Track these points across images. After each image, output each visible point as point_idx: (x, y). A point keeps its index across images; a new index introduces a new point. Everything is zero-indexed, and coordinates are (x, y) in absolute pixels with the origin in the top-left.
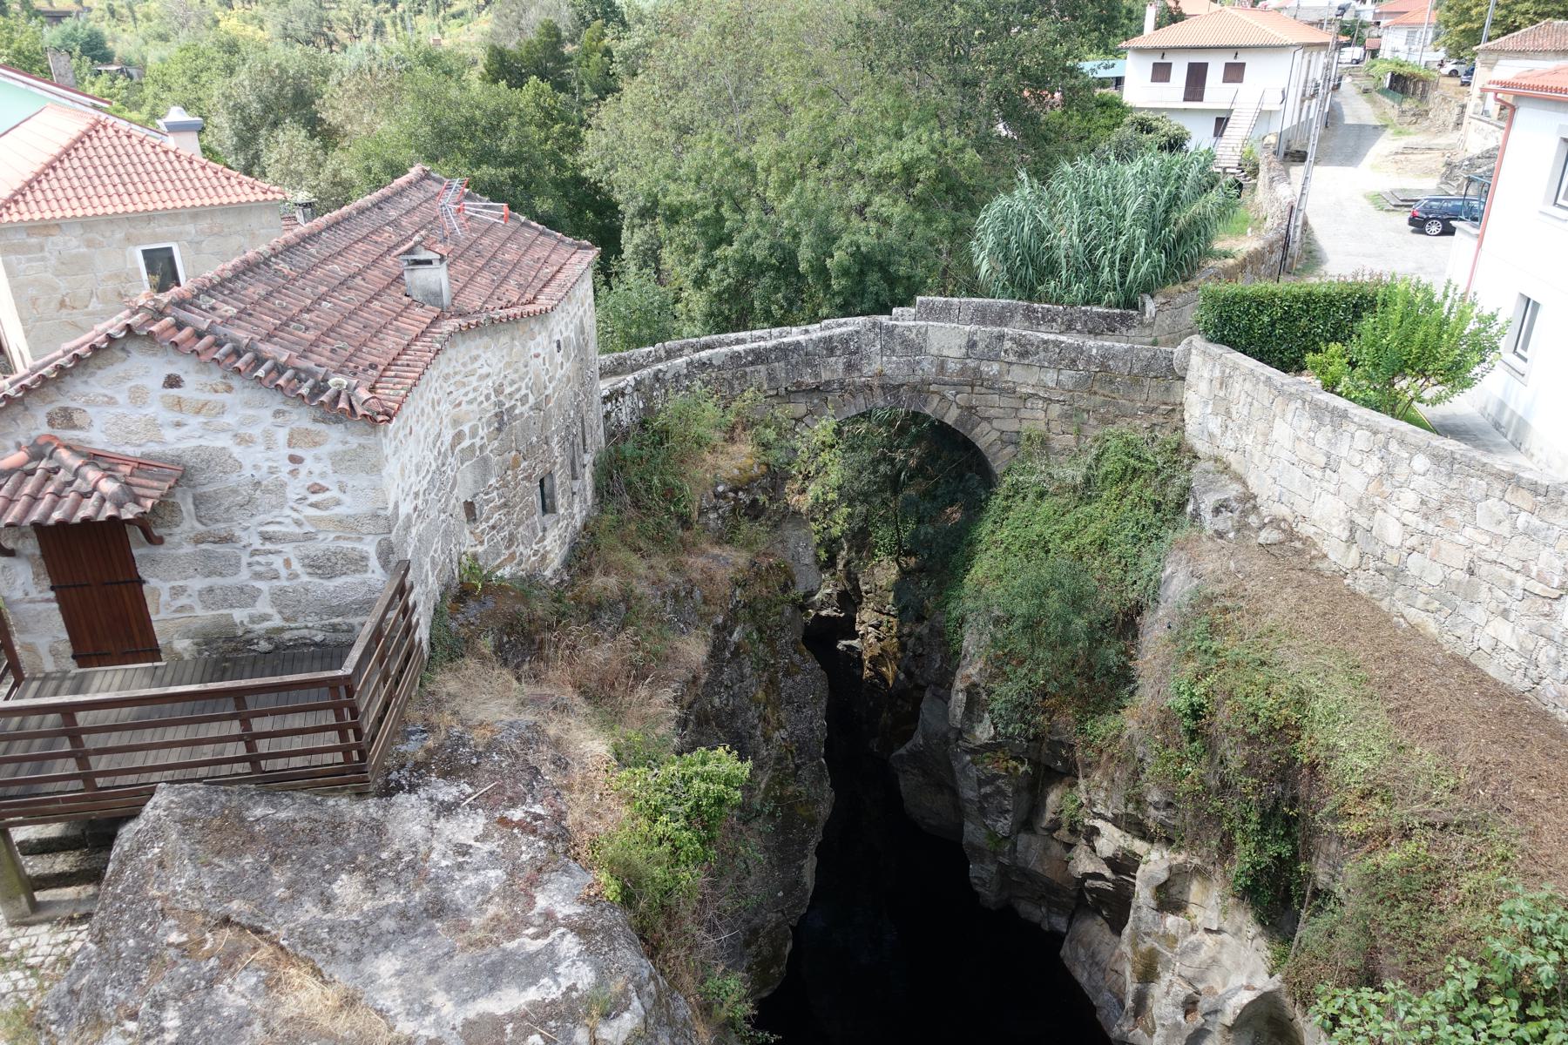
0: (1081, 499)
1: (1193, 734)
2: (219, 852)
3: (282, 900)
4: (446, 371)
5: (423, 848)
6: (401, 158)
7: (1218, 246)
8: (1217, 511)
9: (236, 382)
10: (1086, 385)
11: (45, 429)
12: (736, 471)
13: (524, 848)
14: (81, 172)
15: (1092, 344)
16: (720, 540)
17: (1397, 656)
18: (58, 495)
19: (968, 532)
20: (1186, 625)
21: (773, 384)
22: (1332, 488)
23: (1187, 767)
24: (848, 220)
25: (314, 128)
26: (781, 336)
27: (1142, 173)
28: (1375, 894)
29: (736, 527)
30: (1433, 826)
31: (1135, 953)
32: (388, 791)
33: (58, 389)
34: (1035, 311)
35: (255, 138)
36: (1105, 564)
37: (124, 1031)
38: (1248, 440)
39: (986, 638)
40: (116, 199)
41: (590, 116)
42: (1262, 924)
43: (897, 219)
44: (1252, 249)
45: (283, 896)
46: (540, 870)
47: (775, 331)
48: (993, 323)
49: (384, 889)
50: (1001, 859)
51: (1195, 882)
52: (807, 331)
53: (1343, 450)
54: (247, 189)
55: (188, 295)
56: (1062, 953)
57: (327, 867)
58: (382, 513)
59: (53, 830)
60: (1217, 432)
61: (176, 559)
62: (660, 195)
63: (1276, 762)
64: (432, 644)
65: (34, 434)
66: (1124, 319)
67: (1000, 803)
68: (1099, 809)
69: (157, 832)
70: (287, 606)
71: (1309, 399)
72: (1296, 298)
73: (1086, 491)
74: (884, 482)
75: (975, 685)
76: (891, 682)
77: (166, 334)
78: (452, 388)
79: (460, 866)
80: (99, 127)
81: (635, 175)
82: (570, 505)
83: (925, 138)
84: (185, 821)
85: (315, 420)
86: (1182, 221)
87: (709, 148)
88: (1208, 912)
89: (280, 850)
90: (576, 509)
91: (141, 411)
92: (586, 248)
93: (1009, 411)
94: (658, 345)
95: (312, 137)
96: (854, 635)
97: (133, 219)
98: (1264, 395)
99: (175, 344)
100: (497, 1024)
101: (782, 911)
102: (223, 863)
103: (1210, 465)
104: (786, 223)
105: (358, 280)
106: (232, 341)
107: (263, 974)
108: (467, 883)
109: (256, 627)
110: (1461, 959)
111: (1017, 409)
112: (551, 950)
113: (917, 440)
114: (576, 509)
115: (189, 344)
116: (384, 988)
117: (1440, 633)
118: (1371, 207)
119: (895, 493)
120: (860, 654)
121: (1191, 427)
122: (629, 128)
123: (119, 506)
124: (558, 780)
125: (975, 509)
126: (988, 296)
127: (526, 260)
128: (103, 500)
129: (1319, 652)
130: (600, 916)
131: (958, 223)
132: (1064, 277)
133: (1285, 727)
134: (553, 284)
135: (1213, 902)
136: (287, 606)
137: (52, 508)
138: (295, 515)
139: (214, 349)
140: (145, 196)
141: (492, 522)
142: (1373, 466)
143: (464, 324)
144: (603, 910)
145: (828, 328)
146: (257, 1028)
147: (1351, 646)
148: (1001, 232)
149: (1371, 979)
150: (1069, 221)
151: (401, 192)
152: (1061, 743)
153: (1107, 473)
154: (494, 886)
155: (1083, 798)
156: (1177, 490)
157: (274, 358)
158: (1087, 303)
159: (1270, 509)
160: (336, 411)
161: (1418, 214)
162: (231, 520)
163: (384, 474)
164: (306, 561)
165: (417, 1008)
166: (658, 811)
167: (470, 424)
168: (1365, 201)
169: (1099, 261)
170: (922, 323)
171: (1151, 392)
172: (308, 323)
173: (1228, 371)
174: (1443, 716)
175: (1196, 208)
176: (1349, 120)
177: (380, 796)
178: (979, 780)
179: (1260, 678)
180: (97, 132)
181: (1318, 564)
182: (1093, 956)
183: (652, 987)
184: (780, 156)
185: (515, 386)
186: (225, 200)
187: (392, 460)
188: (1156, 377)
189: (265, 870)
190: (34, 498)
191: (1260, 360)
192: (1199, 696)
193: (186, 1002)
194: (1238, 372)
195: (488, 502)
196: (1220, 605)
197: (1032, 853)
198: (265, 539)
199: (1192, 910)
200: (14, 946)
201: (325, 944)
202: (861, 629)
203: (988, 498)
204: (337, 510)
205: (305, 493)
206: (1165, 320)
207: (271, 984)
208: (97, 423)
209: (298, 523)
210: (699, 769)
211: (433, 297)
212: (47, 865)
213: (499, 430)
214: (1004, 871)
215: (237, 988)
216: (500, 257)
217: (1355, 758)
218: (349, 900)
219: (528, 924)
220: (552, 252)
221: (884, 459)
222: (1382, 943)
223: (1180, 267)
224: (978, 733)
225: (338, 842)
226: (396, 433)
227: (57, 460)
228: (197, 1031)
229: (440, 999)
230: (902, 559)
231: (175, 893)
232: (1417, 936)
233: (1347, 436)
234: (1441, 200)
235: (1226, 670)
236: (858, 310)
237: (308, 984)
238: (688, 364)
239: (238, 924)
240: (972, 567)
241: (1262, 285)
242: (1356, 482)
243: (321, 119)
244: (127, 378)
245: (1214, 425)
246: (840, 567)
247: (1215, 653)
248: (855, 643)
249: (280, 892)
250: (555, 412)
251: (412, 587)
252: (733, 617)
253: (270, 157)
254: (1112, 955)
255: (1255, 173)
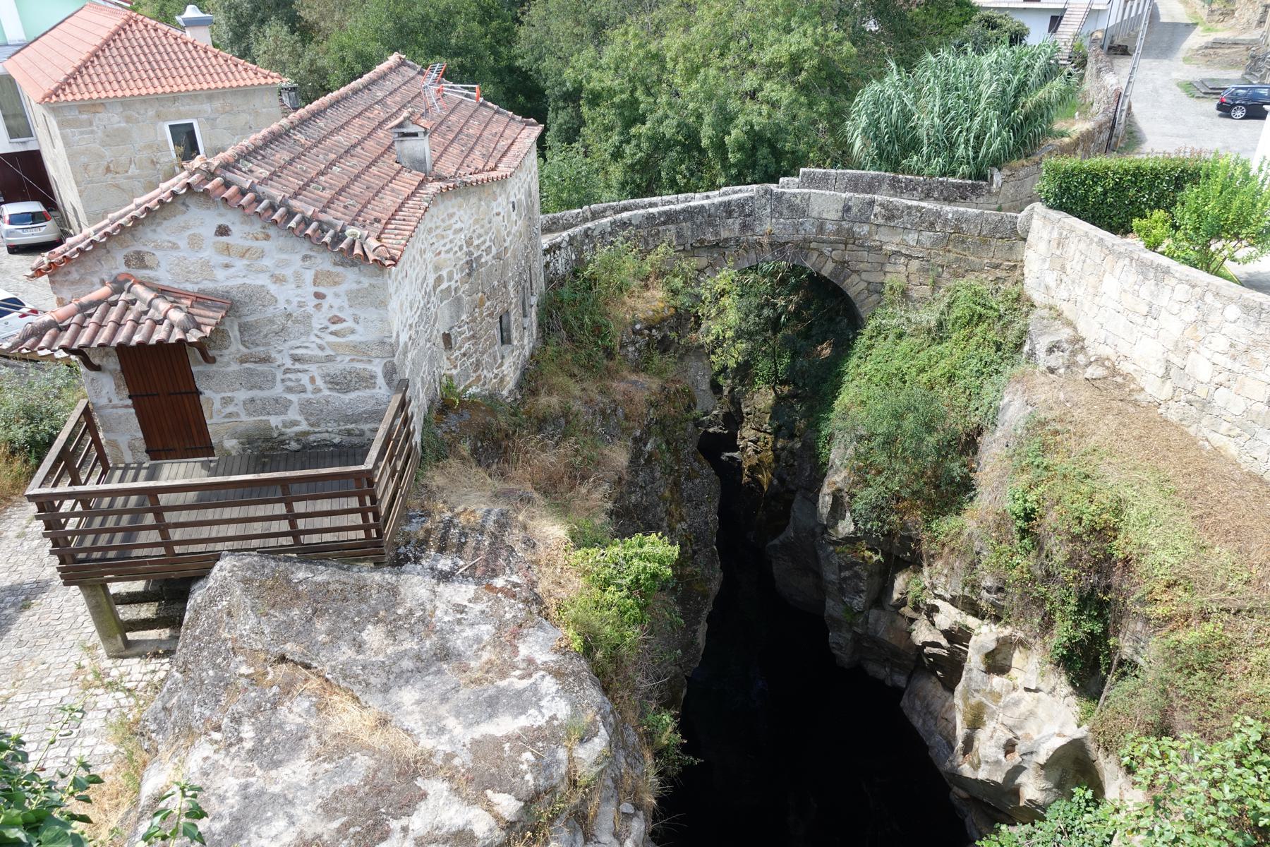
0: (934, 339)
1: (1024, 533)
2: (273, 606)
3: (324, 644)
4: (430, 225)
5: (429, 607)
6: (369, 49)
7: (1058, 126)
8: (1050, 351)
9: (272, 231)
10: (944, 242)
11: (123, 269)
12: (651, 313)
13: (507, 609)
14: (119, 59)
15: (949, 210)
16: (636, 369)
17: (1202, 472)
18: (137, 322)
19: (837, 365)
20: (1020, 444)
21: (681, 241)
22: (1152, 332)
23: (1017, 559)
24: (743, 103)
25: (293, 24)
26: (686, 200)
27: (996, 63)
28: (1174, 665)
29: (649, 359)
30: (1228, 611)
31: (966, 705)
32: (399, 562)
33: (133, 235)
34: (899, 181)
35: (246, 32)
36: (952, 393)
37: (211, 740)
38: (1079, 291)
39: (851, 451)
40: (148, 83)
41: (523, 14)
42: (1073, 685)
43: (785, 102)
44: (1084, 129)
45: (324, 640)
46: (520, 626)
47: (681, 196)
48: (864, 191)
49: (402, 638)
50: (855, 629)
51: (1017, 651)
52: (708, 197)
53: (1163, 300)
54: (251, 74)
55: (232, 160)
56: (902, 704)
57: (357, 619)
58: (387, 340)
59: (138, 586)
60: (1053, 284)
61: (225, 375)
62: (584, 82)
63: (1095, 557)
64: (423, 447)
65: (115, 272)
66: (974, 188)
67: (857, 584)
68: (939, 591)
69: (224, 590)
70: (312, 414)
71: (1136, 257)
72: (1126, 172)
73: (939, 333)
74: (765, 324)
75: (840, 490)
76: (765, 487)
77: (218, 192)
78: (434, 240)
79: (459, 622)
80: (131, 22)
81: (560, 65)
82: (522, 338)
83: (810, 32)
84: (245, 581)
85: (335, 264)
86: (1029, 105)
87: (626, 41)
88: (1028, 675)
89: (319, 605)
90: (526, 342)
91: (198, 254)
92: (532, 124)
93: (876, 265)
94: (585, 207)
95: (293, 33)
96: (736, 448)
97: (162, 99)
98: (1096, 253)
99: (226, 200)
100: (497, 743)
101: (680, 665)
102: (277, 614)
103: (1045, 313)
104: (691, 106)
105: (359, 149)
106: (269, 197)
107: (314, 699)
108: (465, 634)
109: (288, 430)
110: (1247, 718)
111: (883, 264)
112: (534, 689)
113: (795, 289)
114: (526, 342)
115: (236, 200)
116: (408, 713)
117: (1239, 454)
118: (1184, 94)
119: (775, 333)
120: (740, 463)
121: (1030, 281)
122: (555, 25)
123: (186, 331)
124: (529, 556)
125: (844, 348)
126: (859, 169)
127: (486, 133)
128: (172, 326)
129: (1135, 469)
130: (570, 663)
131: (835, 106)
132: (925, 152)
133: (1104, 528)
134: (509, 154)
135: (1033, 667)
136: (312, 414)
137: (133, 332)
138: (319, 341)
139: (255, 204)
140: (170, 79)
141: (463, 350)
142: (1190, 314)
143: (444, 187)
144: (572, 659)
145: (725, 194)
146: (313, 740)
147: (1163, 464)
148: (873, 114)
149: (1164, 730)
150: (931, 104)
151: (383, 76)
152: (910, 539)
153: (957, 318)
154: (486, 638)
155: (926, 582)
156: (1016, 333)
157: (302, 212)
158: (944, 175)
159: (1095, 350)
160: (351, 257)
161: (1225, 100)
162: (268, 344)
163: (389, 308)
164: (328, 379)
165: (434, 729)
166: (607, 583)
167: (448, 270)
168: (1179, 90)
169: (956, 140)
170: (806, 191)
171: (996, 251)
172: (324, 184)
173: (1065, 233)
174: (1240, 522)
175: (1042, 94)
176: (1164, 19)
177: (393, 566)
178: (840, 566)
179: (1085, 489)
180: (130, 26)
181: (1136, 396)
182: (928, 706)
183: (611, 719)
184: (686, 48)
185: (482, 239)
186: (235, 84)
187: (394, 297)
188: (1002, 238)
189: (309, 620)
190: (118, 325)
191: (1093, 224)
192: (1032, 502)
193: (257, 719)
194: (1074, 234)
195: (461, 333)
196: (1052, 428)
197: (879, 623)
198: (295, 360)
199: (1013, 672)
200: (114, 673)
201: (361, 678)
202: (741, 444)
203: (855, 338)
204: (351, 338)
205: (326, 323)
206: (1009, 190)
207: (320, 708)
208: (163, 264)
209: (321, 348)
210: (639, 551)
211: (418, 164)
212: (135, 613)
213: (469, 275)
214: (857, 639)
215: (295, 710)
216: (465, 130)
217: (1162, 555)
218: (376, 645)
219: (514, 667)
220: (506, 127)
221: (767, 305)
222: (1178, 703)
223: (1024, 144)
224: (840, 529)
225: (362, 600)
226: (397, 275)
227: (134, 294)
228: (267, 741)
229: (451, 722)
230: (777, 387)
231: (242, 636)
232: (1209, 699)
233: (1167, 290)
234: (1246, 89)
235: (1055, 481)
236: (749, 179)
237: (349, 708)
238: (612, 223)
239: (292, 661)
240: (840, 394)
241: (1098, 160)
242: (1172, 327)
243: (300, 17)
244: (186, 228)
245: (1051, 279)
246: (726, 393)
247: (1046, 468)
248: (736, 454)
249: (322, 638)
250: (511, 261)
251: (410, 401)
252: (647, 432)
253: (259, 49)
254: (943, 706)
255: (1083, 64)
